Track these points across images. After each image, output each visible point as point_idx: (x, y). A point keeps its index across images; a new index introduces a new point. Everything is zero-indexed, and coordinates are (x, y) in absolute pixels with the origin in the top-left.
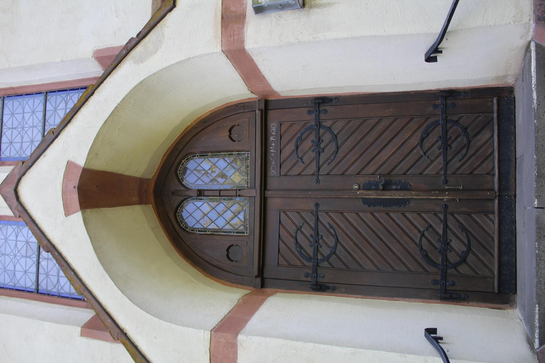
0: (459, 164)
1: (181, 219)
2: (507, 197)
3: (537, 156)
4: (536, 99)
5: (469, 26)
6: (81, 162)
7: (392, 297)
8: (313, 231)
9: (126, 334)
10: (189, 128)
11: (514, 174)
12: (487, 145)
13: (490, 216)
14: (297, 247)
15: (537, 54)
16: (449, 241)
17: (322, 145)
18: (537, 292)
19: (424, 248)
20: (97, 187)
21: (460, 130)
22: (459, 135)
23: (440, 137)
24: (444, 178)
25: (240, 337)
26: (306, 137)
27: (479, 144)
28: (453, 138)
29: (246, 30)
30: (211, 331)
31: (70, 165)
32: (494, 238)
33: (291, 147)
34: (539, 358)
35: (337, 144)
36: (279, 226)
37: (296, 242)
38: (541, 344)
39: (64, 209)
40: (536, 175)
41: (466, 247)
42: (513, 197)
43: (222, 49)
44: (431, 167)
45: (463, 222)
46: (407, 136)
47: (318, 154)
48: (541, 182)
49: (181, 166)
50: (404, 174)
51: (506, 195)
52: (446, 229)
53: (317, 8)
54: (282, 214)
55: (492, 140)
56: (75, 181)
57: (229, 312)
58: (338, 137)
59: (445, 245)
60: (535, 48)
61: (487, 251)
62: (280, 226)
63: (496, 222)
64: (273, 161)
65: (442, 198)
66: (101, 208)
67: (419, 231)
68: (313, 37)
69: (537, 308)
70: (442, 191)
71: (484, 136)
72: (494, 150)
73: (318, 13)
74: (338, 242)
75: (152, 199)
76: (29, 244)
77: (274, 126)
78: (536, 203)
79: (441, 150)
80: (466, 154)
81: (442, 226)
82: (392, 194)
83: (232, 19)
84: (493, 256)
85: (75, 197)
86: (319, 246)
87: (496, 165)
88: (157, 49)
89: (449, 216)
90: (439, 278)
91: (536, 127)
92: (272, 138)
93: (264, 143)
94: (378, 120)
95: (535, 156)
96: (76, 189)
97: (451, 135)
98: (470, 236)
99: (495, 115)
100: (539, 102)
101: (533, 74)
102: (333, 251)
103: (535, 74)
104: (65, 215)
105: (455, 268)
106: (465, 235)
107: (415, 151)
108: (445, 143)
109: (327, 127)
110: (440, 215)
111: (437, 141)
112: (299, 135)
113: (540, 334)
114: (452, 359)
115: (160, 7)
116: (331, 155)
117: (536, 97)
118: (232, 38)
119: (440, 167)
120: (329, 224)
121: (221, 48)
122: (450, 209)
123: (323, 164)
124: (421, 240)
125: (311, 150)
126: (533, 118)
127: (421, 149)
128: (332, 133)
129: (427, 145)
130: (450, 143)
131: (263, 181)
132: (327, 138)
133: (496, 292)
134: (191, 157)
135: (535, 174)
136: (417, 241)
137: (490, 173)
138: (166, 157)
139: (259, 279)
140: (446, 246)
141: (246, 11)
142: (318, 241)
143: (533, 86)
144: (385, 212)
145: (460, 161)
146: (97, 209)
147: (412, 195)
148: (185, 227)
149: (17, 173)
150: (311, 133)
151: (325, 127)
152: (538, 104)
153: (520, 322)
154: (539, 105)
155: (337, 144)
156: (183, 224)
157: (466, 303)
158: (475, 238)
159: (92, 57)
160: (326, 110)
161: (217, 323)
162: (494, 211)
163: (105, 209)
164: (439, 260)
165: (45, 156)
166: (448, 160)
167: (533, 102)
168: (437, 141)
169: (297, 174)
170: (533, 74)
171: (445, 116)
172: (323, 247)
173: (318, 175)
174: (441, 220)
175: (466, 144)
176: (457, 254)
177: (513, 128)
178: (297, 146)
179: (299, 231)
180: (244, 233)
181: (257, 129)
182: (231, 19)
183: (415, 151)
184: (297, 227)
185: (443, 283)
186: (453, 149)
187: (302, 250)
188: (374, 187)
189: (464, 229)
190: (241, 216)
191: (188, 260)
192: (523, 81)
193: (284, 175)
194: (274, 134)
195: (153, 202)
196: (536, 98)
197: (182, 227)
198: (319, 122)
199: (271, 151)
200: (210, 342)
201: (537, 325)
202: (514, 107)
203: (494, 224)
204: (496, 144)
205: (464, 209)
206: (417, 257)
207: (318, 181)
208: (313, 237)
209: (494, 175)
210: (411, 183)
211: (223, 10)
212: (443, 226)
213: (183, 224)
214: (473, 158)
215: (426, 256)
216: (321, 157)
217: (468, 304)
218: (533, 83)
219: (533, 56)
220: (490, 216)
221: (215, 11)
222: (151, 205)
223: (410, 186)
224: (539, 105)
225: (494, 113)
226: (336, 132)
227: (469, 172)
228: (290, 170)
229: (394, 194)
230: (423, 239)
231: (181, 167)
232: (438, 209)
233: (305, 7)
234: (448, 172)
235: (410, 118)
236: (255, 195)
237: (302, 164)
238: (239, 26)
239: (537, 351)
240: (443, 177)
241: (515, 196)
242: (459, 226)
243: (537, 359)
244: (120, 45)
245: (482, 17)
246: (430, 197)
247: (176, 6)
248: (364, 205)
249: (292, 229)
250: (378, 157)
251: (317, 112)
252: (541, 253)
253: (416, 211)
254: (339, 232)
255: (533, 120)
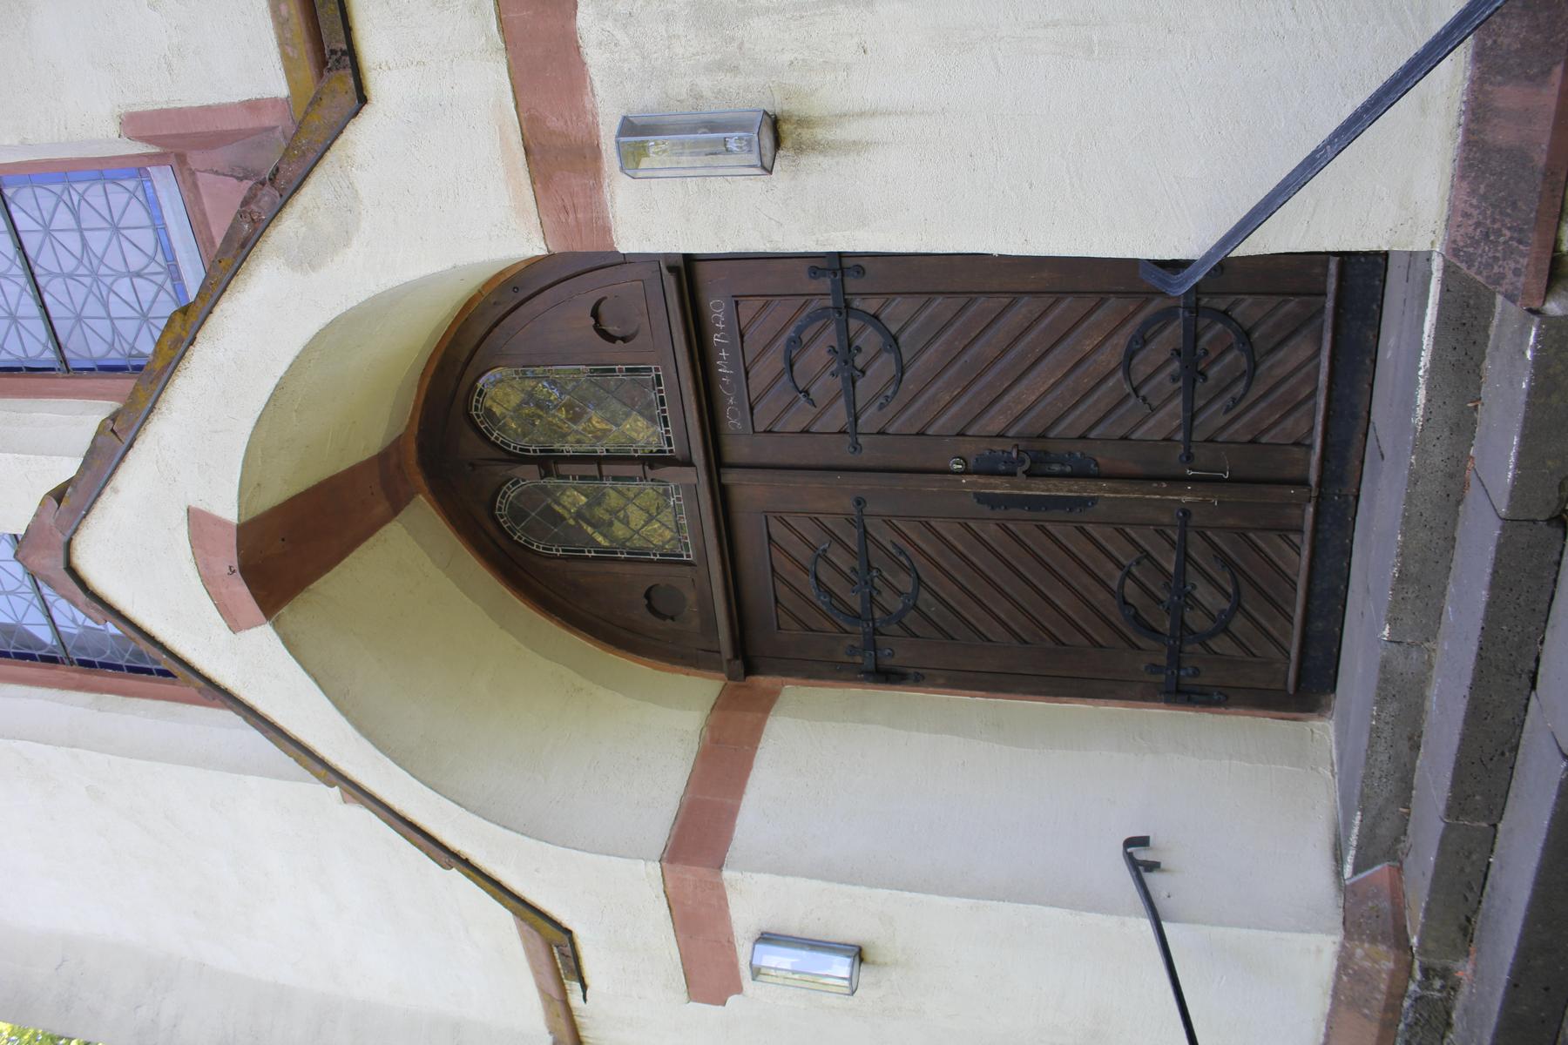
0: (1222, 420)
1: (509, 524)
2: (1336, 498)
3: (1403, 534)
4: (1422, 406)
5: (1267, 246)
6: (229, 512)
7: (1057, 695)
8: (856, 559)
9: (467, 860)
10: (476, 304)
11: (1361, 449)
12: (1301, 375)
13: (1292, 536)
14: (819, 596)
15: (1445, 289)
16: (1189, 588)
17: (859, 361)
18: (1362, 790)
19: (1130, 601)
20: (283, 540)
21: (1233, 336)
22: (1230, 348)
23: (1178, 353)
24: (1182, 451)
25: (727, 874)
26: (812, 340)
27: (1279, 372)
28: (1213, 355)
29: (609, 198)
30: (660, 861)
31: (198, 521)
32: (1296, 585)
33: (773, 362)
34: (1346, 906)
35: (899, 359)
36: (770, 549)
37: (818, 585)
38: (1356, 871)
39: (221, 615)
40: (1395, 576)
41: (1229, 601)
42: (1351, 498)
43: (547, 245)
44: (1152, 422)
45: (1225, 548)
46: (1089, 345)
47: (851, 384)
48: (1405, 590)
49: (476, 397)
50: (1083, 437)
51: (1335, 494)
52: (1185, 564)
53: (821, 152)
54: (773, 523)
55: (1314, 362)
56: (227, 557)
57: (687, 784)
58: (901, 340)
59: (1179, 598)
60: (1441, 272)
61: (1278, 610)
62: (772, 548)
63: (1305, 552)
64: (729, 397)
65: (1176, 498)
66: (311, 587)
67: (1119, 565)
68: (817, 241)
69: (1358, 817)
70: (1178, 480)
71: (1299, 350)
72: (1316, 388)
73: (825, 171)
74: (919, 584)
75: (420, 480)
76: (19, 318)
77: (717, 306)
78: (1386, 632)
79: (1180, 384)
80: (1243, 396)
81: (1174, 557)
82: (1050, 486)
83: (559, 159)
84: (1290, 619)
85: (241, 590)
86: (875, 593)
87: (1319, 429)
88: (347, 232)
89: (1193, 537)
90: (1162, 660)
91: (1411, 474)
92: (716, 337)
93: (697, 356)
94: (1011, 299)
95: (1400, 536)
96: (238, 574)
97: (1207, 348)
98: (1240, 579)
99: (1330, 304)
100: (1431, 412)
101: (1425, 342)
102: (911, 603)
103: (1432, 343)
104: (230, 628)
105: (1204, 644)
106: (1228, 576)
107: (1111, 383)
108: (1189, 367)
109: (868, 314)
110: (1169, 532)
111: (1168, 362)
112: (790, 332)
113: (1356, 857)
114: (1171, 921)
115: (315, 96)
116: (886, 386)
117: (1424, 401)
118: (571, 216)
119: (1174, 424)
120: (894, 545)
121: (543, 243)
122: (1195, 520)
123: (865, 408)
124: (1122, 585)
125: (829, 372)
126: (1409, 448)
127: (1125, 379)
128: (883, 330)
129: (1141, 368)
130: (1203, 366)
131: (706, 417)
132: (868, 339)
133: (1291, 692)
134: (515, 448)
135: (1395, 573)
136: (1114, 585)
137: (1302, 444)
138: (428, 380)
139: (739, 662)
140: (1183, 598)
141: (598, 136)
142: (869, 582)
143: (1421, 373)
144: (1034, 523)
145: (1228, 410)
146: (302, 593)
147: (1101, 489)
148: (525, 541)
149: (52, 524)
150: (824, 327)
151: (862, 314)
152: (1427, 418)
153: (1331, 777)
154: (1428, 420)
155: (899, 359)
156: (519, 534)
157: (1223, 709)
158: (1254, 584)
159: (120, 136)
160: (860, 266)
161: (668, 831)
162: (1303, 527)
163: (321, 580)
164: (1166, 625)
165: (116, 491)
166: (1196, 409)
167: (1415, 410)
168: (1168, 362)
169: (799, 430)
170: (1427, 341)
171: (1194, 298)
172: (884, 594)
173: (856, 433)
174: (1172, 543)
175: (1245, 371)
176: (1209, 614)
177: (1371, 338)
178: (791, 361)
179: (819, 559)
180: (682, 556)
181: (674, 330)
182: (557, 158)
183: (1111, 384)
184: (815, 552)
185: (1173, 673)
186: (1211, 382)
187: (833, 599)
188: (1004, 468)
189: (1227, 563)
190: (667, 517)
191: (553, 615)
192: (1407, 281)
193: (765, 432)
194: (722, 326)
195: (426, 488)
196: (1425, 405)
197: (516, 541)
198: (845, 300)
199: (720, 370)
200: (664, 880)
201: (1355, 843)
202: (1382, 284)
203: (1299, 555)
204: (1323, 377)
205: (1231, 521)
206: (1113, 619)
207: (856, 447)
208: (857, 573)
209: (1310, 447)
210: (1099, 460)
211: (524, 127)
212: (1178, 556)
213: (519, 534)
214: (1263, 405)
215: (1137, 620)
216: (857, 390)
217: (1227, 711)
218: (1422, 364)
219: (1434, 296)
220: (1292, 536)
221: (500, 130)
222: (421, 496)
223: (1097, 464)
224: (1428, 420)
225: (1326, 295)
226: (894, 329)
227: (1249, 437)
228: (777, 419)
229: (1056, 486)
230: (1128, 581)
231: (501, 503)
232: (1166, 519)
233: (782, 145)
234: (1195, 437)
235: (1098, 299)
236: (695, 480)
237: (809, 407)
238: (587, 182)
239: (1347, 882)
240: (1182, 446)
241: (1357, 498)
242: (1215, 556)
243: (1341, 910)
244: (198, 105)
245: (1306, 225)
246: (1147, 496)
247: (368, 98)
248: (980, 506)
249: (803, 554)
250: (1013, 393)
251: (836, 275)
252: (1382, 726)
253: (1112, 523)
254: (920, 563)
255: (1409, 453)
